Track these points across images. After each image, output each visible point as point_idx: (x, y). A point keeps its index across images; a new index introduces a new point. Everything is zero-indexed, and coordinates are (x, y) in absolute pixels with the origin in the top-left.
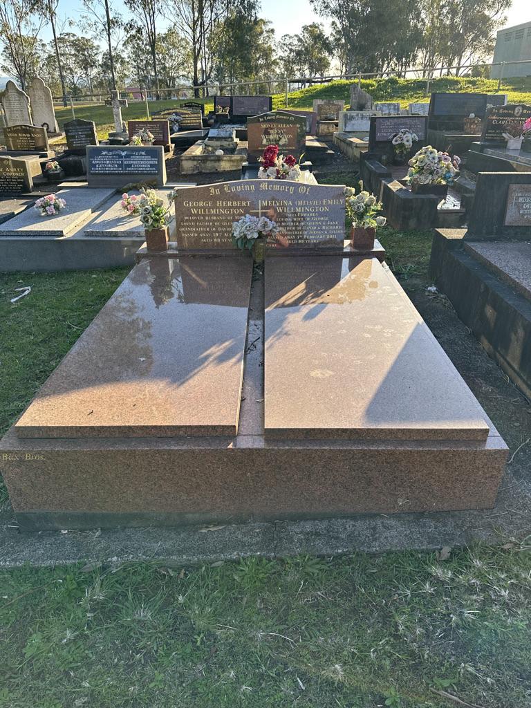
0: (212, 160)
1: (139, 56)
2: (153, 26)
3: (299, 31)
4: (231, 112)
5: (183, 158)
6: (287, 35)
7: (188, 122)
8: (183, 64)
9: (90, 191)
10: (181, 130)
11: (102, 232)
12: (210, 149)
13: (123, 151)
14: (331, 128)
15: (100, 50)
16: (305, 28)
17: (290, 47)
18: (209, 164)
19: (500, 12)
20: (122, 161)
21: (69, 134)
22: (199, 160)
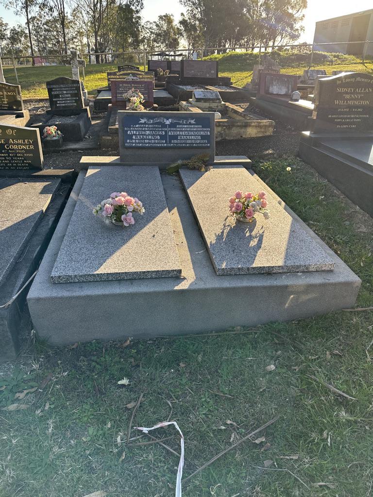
0: (238, 126)
1: (39, 32)
2: (62, 6)
3: (157, 19)
6: (148, 22)
8: (73, 40)
9: (119, 169)
11: (248, 269)
13: (168, 119)
15: (8, 27)
16: (161, 17)
17: (151, 30)
18: (235, 131)
19: (300, 11)
20: (166, 132)
21: (53, 93)
22: (224, 126)
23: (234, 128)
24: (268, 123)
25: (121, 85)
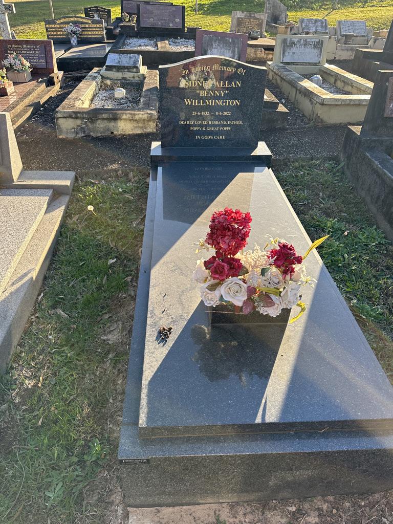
4: (138, 21)
5: (59, 115)
7: (89, 34)
10: (82, 42)
12: (109, 82)
14: (258, 52)
18: (101, 125)
22: (84, 118)
23: (99, 122)
24: (146, 115)
25: (9, 46)
